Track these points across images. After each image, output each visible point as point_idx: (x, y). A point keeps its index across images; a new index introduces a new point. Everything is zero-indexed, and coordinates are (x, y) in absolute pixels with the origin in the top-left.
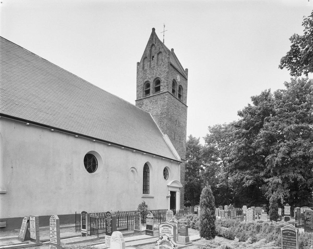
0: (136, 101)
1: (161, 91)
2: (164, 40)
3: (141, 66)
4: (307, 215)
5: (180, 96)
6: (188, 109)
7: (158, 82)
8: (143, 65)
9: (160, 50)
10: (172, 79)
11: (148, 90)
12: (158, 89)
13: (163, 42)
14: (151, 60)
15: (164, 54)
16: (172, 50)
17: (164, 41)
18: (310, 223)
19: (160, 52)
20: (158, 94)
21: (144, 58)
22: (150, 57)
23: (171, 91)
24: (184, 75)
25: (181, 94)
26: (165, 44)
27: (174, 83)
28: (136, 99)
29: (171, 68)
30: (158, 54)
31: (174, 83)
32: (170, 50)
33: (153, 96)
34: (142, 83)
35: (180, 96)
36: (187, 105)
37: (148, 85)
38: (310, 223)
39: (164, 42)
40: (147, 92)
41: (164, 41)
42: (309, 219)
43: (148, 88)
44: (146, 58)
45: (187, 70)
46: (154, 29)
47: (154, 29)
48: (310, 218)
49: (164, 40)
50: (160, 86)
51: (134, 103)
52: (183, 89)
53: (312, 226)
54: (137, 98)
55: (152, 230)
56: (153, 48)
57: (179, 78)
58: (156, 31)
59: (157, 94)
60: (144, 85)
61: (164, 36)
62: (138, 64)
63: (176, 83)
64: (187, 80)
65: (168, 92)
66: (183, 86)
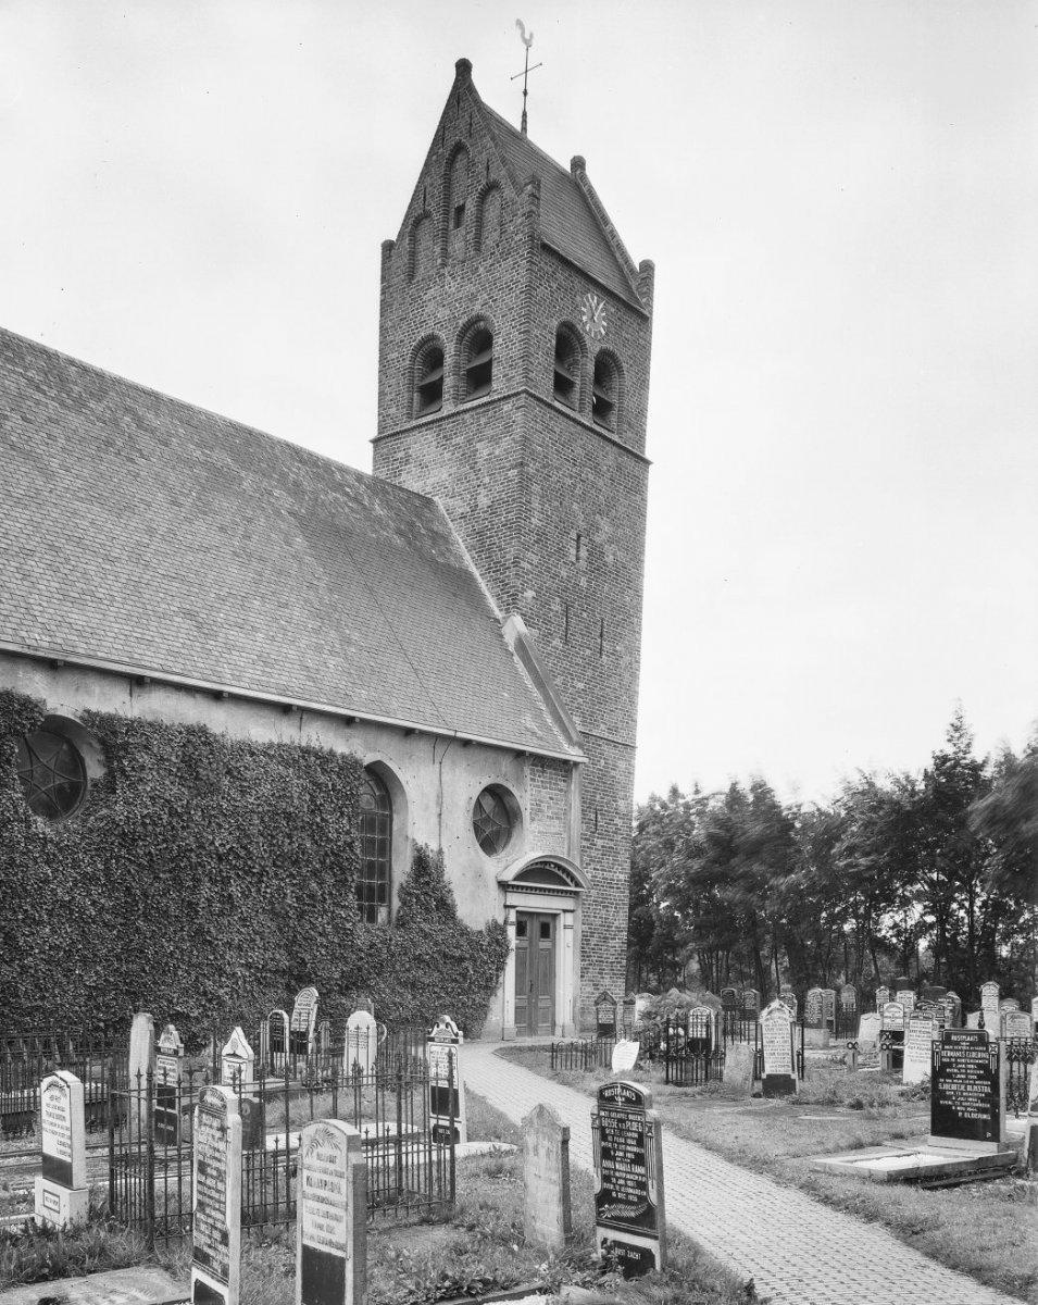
0: (375, 441)
1: (494, 386)
2: (525, 115)
3: (402, 263)
4: (943, 1049)
5: (601, 409)
6: (656, 481)
7: (478, 338)
8: (413, 254)
9: (493, 176)
10: (555, 323)
11: (434, 383)
12: (479, 378)
13: (518, 126)
14: (451, 226)
15: (508, 192)
16: (578, 163)
17: (524, 121)
18: (954, 1087)
19: (492, 187)
20: (479, 406)
21: (415, 221)
22: (446, 213)
23: (545, 388)
24: (630, 296)
25: (614, 399)
26: (531, 136)
27: (567, 342)
28: (374, 433)
29: (546, 264)
30: (483, 196)
31: (567, 342)
32: (568, 168)
33: (453, 415)
34: (408, 350)
35: (601, 409)
36: (648, 455)
37: (431, 355)
38: (954, 1087)
39: (524, 129)
40: (431, 394)
41: (524, 121)
42: (949, 1065)
43: (433, 375)
44: (426, 215)
45: (647, 267)
46: (464, 68)
47: (464, 68)
48: (957, 1063)
49: (525, 115)
50: (489, 363)
51: (361, 459)
52: (620, 369)
53: (961, 1105)
54: (381, 428)
55: (174, 1108)
56: (460, 163)
57: (594, 319)
58: (477, 77)
59: (476, 403)
60: (413, 359)
61: (525, 93)
62: (388, 247)
63: (580, 338)
64: (644, 319)
65: (525, 391)
66: (623, 356)
